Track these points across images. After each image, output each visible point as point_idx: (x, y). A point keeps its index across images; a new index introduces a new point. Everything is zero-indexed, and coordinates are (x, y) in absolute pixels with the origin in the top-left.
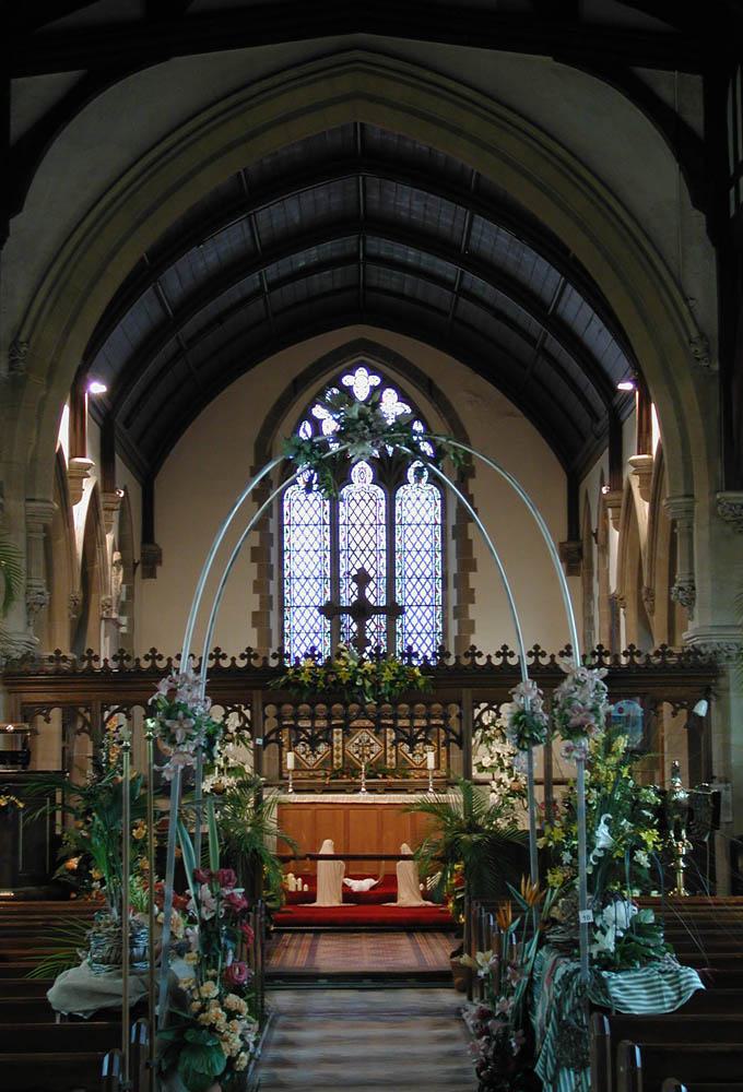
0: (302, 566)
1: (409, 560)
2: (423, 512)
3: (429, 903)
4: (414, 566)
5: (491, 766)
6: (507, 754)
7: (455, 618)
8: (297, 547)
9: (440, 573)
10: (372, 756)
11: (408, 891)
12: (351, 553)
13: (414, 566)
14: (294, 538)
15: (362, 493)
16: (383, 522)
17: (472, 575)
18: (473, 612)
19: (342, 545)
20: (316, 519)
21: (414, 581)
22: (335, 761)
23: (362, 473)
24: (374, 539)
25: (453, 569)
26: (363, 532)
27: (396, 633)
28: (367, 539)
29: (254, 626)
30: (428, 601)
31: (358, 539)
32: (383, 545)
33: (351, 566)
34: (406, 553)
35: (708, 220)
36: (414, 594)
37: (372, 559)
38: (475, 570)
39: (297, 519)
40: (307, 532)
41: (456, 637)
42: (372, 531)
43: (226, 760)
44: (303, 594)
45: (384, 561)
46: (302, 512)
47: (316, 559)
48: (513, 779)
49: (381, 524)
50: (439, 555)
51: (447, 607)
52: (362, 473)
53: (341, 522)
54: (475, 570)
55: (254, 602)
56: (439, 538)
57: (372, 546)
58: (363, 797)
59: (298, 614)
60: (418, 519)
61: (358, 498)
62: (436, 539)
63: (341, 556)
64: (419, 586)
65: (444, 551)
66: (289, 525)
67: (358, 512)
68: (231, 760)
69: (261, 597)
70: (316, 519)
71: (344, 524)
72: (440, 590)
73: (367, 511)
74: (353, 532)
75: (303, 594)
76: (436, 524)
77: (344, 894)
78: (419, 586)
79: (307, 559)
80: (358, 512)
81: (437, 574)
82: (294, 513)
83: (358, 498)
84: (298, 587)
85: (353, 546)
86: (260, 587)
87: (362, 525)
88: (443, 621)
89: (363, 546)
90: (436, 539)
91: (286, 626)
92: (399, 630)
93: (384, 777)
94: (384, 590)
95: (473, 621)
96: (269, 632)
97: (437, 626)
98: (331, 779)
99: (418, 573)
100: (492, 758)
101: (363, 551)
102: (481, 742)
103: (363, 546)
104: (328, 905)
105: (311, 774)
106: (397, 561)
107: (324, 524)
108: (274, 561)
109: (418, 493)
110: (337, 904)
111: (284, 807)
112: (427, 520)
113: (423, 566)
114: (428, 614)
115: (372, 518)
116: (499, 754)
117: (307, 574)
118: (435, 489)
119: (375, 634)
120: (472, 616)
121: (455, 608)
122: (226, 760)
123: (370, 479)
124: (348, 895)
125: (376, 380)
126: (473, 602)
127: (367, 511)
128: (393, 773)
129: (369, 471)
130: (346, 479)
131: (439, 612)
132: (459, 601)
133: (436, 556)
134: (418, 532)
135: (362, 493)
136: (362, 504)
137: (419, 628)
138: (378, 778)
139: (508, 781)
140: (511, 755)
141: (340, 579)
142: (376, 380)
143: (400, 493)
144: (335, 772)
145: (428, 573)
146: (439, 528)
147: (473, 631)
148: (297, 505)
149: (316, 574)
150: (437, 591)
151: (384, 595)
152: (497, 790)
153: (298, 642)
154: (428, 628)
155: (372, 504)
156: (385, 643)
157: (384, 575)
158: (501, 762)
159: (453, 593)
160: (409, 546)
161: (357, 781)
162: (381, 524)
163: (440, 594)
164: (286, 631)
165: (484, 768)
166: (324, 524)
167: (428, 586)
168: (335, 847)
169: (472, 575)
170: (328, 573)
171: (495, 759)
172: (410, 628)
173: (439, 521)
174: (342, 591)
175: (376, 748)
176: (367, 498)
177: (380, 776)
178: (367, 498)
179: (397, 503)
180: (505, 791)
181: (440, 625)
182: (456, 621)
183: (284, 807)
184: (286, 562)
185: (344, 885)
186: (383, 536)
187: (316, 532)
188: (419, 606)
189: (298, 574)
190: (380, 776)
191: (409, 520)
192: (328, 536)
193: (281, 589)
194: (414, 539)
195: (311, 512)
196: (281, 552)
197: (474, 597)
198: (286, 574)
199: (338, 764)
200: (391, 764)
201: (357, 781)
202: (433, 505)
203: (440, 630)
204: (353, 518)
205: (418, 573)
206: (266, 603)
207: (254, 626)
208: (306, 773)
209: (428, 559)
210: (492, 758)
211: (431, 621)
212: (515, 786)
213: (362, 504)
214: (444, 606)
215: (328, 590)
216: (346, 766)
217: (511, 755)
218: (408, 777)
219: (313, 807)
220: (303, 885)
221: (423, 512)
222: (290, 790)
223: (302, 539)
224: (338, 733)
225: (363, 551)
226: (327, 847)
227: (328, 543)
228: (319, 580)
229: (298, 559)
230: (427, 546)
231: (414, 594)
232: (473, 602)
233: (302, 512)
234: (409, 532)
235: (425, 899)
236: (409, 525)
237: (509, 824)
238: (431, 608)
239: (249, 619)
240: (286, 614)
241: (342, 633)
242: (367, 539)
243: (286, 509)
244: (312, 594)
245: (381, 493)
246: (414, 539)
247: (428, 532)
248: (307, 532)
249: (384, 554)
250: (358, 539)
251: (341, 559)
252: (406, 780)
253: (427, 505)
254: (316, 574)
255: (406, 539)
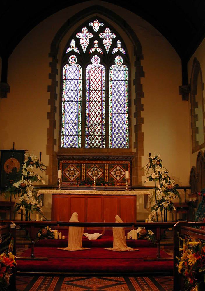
0: (70, 96)
1: (115, 94)
2: (121, 75)
3: (131, 249)
4: (117, 97)
5: (156, 178)
6: (163, 172)
7: (134, 148)
8: (68, 88)
9: (128, 100)
10: (98, 176)
11: (119, 241)
12: (90, 91)
13: (117, 97)
14: (67, 85)
15: (96, 68)
16: (104, 79)
17: (142, 99)
18: (143, 114)
19: (87, 88)
20: (76, 77)
21: (117, 103)
22: (82, 178)
23: (96, 61)
24: (100, 86)
25: (134, 97)
26: (96, 83)
27: (109, 124)
28: (97, 86)
29: (48, 118)
30: (123, 111)
31: (94, 86)
32: (104, 88)
33: (90, 97)
34: (114, 92)
35: (178, 270)
36: (117, 108)
37: (99, 94)
38: (144, 97)
39: (68, 77)
40: (72, 83)
41: (135, 126)
42: (99, 83)
43: (28, 173)
44: (70, 107)
45: (104, 95)
46: (70, 75)
47: (76, 93)
48: (168, 183)
49: (103, 80)
50: (128, 93)
51: (131, 114)
52: (96, 61)
53: (87, 79)
54: (144, 97)
55: (48, 109)
56: (128, 86)
57: (99, 89)
58: (94, 192)
59: (68, 116)
60: (119, 78)
61: (94, 69)
62: (126, 87)
63: (86, 93)
64: (119, 105)
65: (130, 91)
66: (65, 79)
67: (94, 75)
68: (31, 173)
69: (51, 106)
70: (76, 77)
71: (88, 80)
72: (128, 107)
73: (98, 75)
74: (92, 83)
75: (70, 107)
76: (126, 80)
77: (83, 242)
78: (119, 105)
79: (72, 94)
80: (94, 75)
81: (126, 101)
82: (67, 75)
83: (94, 69)
84: (68, 104)
85: (92, 88)
86: (51, 102)
87: (95, 80)
88: (129, 120)
89: (95, 88)
90: (126, 87)
91: (62, 121)
92: (110, 123)
93: (104, 185)
94: (104, 107)
95: (143, 118)
96: (55, 122)
97: (126, 122)
98: (80, 185)
99: (119, 100)
100: (156, 174)
101: (95, 91)
102: (150, 168)
103: (95, 88)
104: (76, 249)
105: (72, 183)
106: (110, 95)
107: (80, 79)
108: (58, 92)
109: (119, 68)
110: (79, 248)
111: (55, 196)
112: (123, 78)
113: (121, 97)
114: (123, 117)
115: (99, 77)
116: (159, 172)
117: (72, 99)
118: (126, 67)
119: (100, 125)
120: (142, 103)
121: (134, 142)
122: (28, 173)
123: (99, 63)
124: (86, 242)
125: (102, 25)
126: (143, 110)
127: (98, 75)
128: (107, 183)
129: (99, 60)
130: (89, 61)
131: (127, 116)
132: (136, 110)
133: (126, 94)
134: (119, 84)
135: (96, 68)
136: (96, 72)
137: (119, 123)
138: (101, 185)
139: (165, 184)
140: (165, 173)
141: (85, 102)
142: (102, 25)
143: (111, 68)
144: (82, 182)
145: (123, 100)
146: (127, 82)
147: (143, 123)
148: (69, 72)
149: (76, 99)
150: (126, 108)
151: (104, 109)
152: (160, 188)
153: (67, 127)
154: (123, 123)
155: (100, 72)
156: (104, 129)
157: (104, 100)
158: (161, 177)
159: (134, 107)
160: (115, 89)
161: (92, 186)
162: (103, 80)
163: (128, 109)
164: (62, 123)
165: (152, 179)
166: (80, 79)
167: (123, 105)
168: (79, 218)
169: (142, 99)
170: (81, 99)
171: (157, 175)
172: (115, 122)
173: (128, 79)
174: (86, 107)
175: (100, 173)
176: (98, 69)
177: (102, 184)
178: (98, 69)
179: (110, 93)
180: (165, 189)
181: (128, 122)
182: (135, 119)
183: (55, 196)
184: (63, 94)
185: (84, 235)
186: (104, 85)
187: (76, 83)
188: (119, 114)
189: (68, 99)
190: (102, 184)
191: (115, 78)
192: (81, 84)
193: (61, 106)
194: (117, 86)
195: (74, 75)
196: (61, 90)
197: (143, 108)
198: (63, 99)
199: (83, 179)
200: (106, 180)
201: (92, 186)
202: (125, 73)
203: (128, 123)
204: (92, 77)
205: (119, 100)
206: (54, 109)
207: (48, 118)
208: (69, 183)
209: (123, 94)
210: (156, 174)
211: (124, 120)
212: (169, 187)
213: (96, 72)
214: (130, 114)
215: (81, 106)
216: (87, 180)
217: (165, 173)
218: (114, 185)
219: (69, 196)
220: (62, 236)
221: (121, 75)
222: (59, 188)
223: (70, 85)
224: (83, 166)
225: (95, 91)
226: (74, 218)
227: (81, 87)
228: (77, 91)
229: (68, 93)
230: (123, 89)
231: (117, 108)
232: (143, 110)
233: (70, 75)
234: (115, 83)
235: (128, 246)
236: (115, 80)
237: (168, 205)
238: (124, 114)
239: (46, 116)
240: (63, 116)
241: (86, 124)
242: (97, 86)
243: (64, 73)
244: (74, 108)
245: (103, 68)
246: (117, 86)
247: (123, 84)
248: (72, 83)
249: (104, 92)
250: (94, 86)
251: (87, 94)
252: (113, 186)
253: (123, 73)
254: (76, 99)
255: (114, 86)
